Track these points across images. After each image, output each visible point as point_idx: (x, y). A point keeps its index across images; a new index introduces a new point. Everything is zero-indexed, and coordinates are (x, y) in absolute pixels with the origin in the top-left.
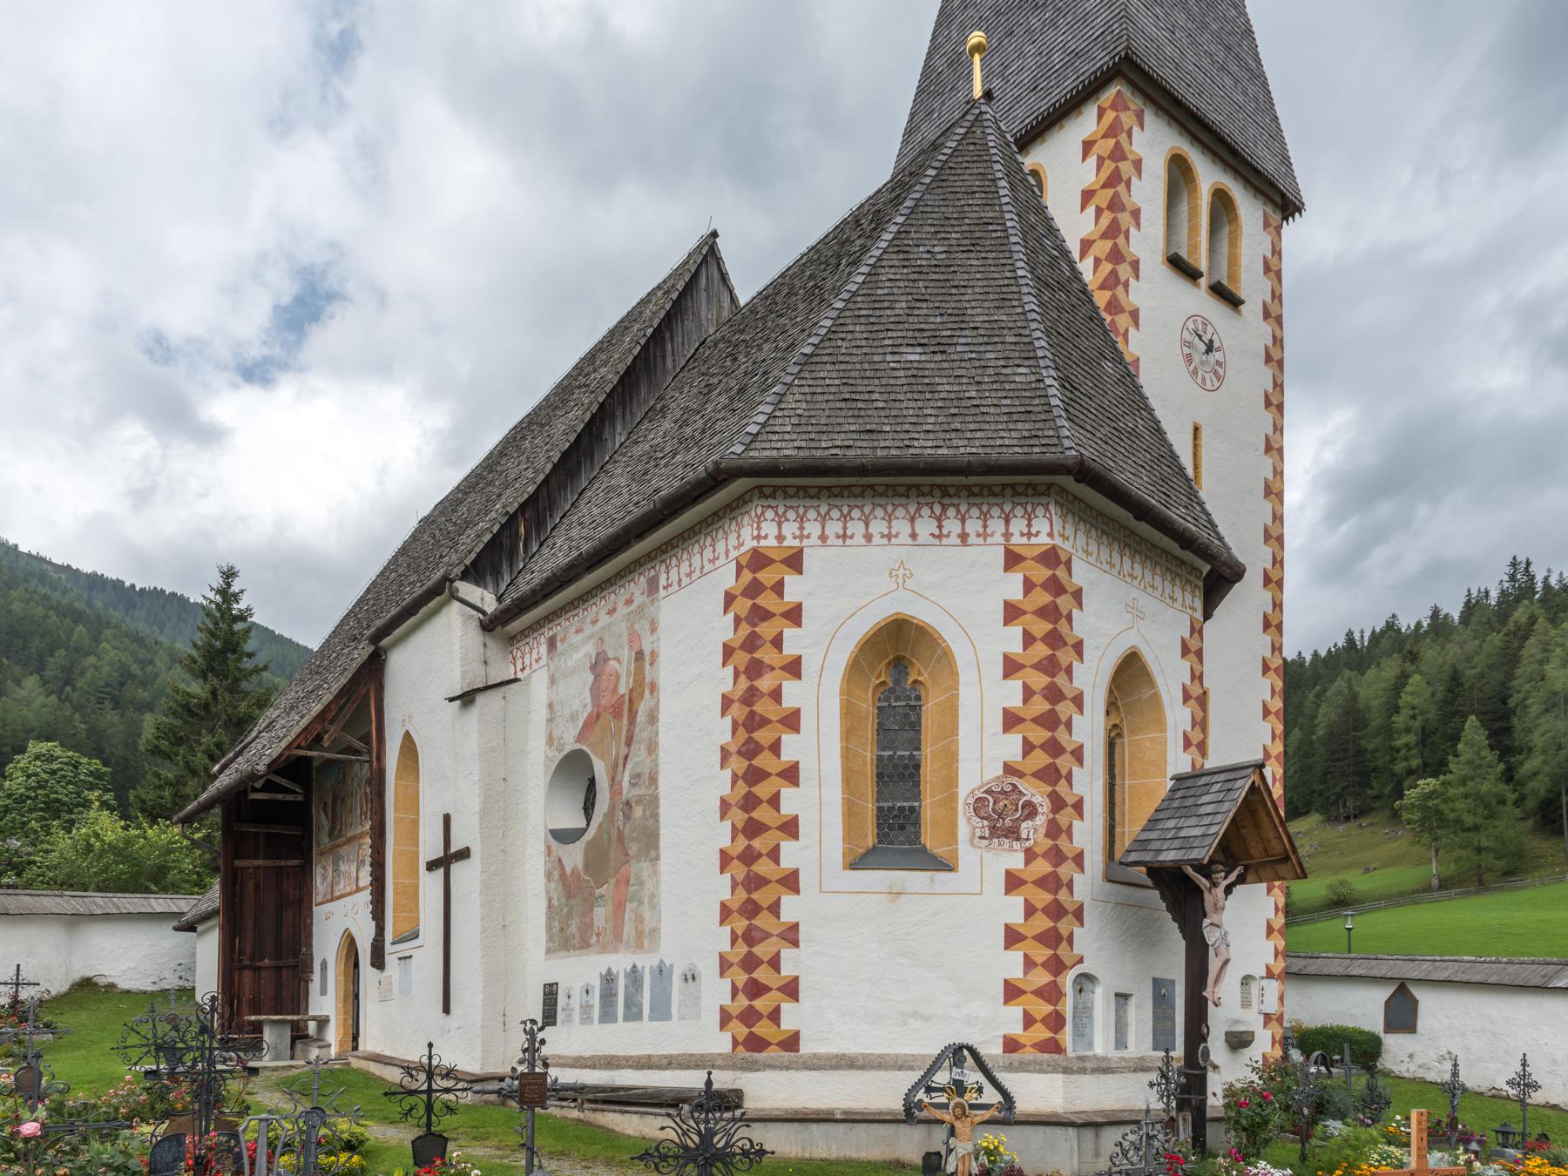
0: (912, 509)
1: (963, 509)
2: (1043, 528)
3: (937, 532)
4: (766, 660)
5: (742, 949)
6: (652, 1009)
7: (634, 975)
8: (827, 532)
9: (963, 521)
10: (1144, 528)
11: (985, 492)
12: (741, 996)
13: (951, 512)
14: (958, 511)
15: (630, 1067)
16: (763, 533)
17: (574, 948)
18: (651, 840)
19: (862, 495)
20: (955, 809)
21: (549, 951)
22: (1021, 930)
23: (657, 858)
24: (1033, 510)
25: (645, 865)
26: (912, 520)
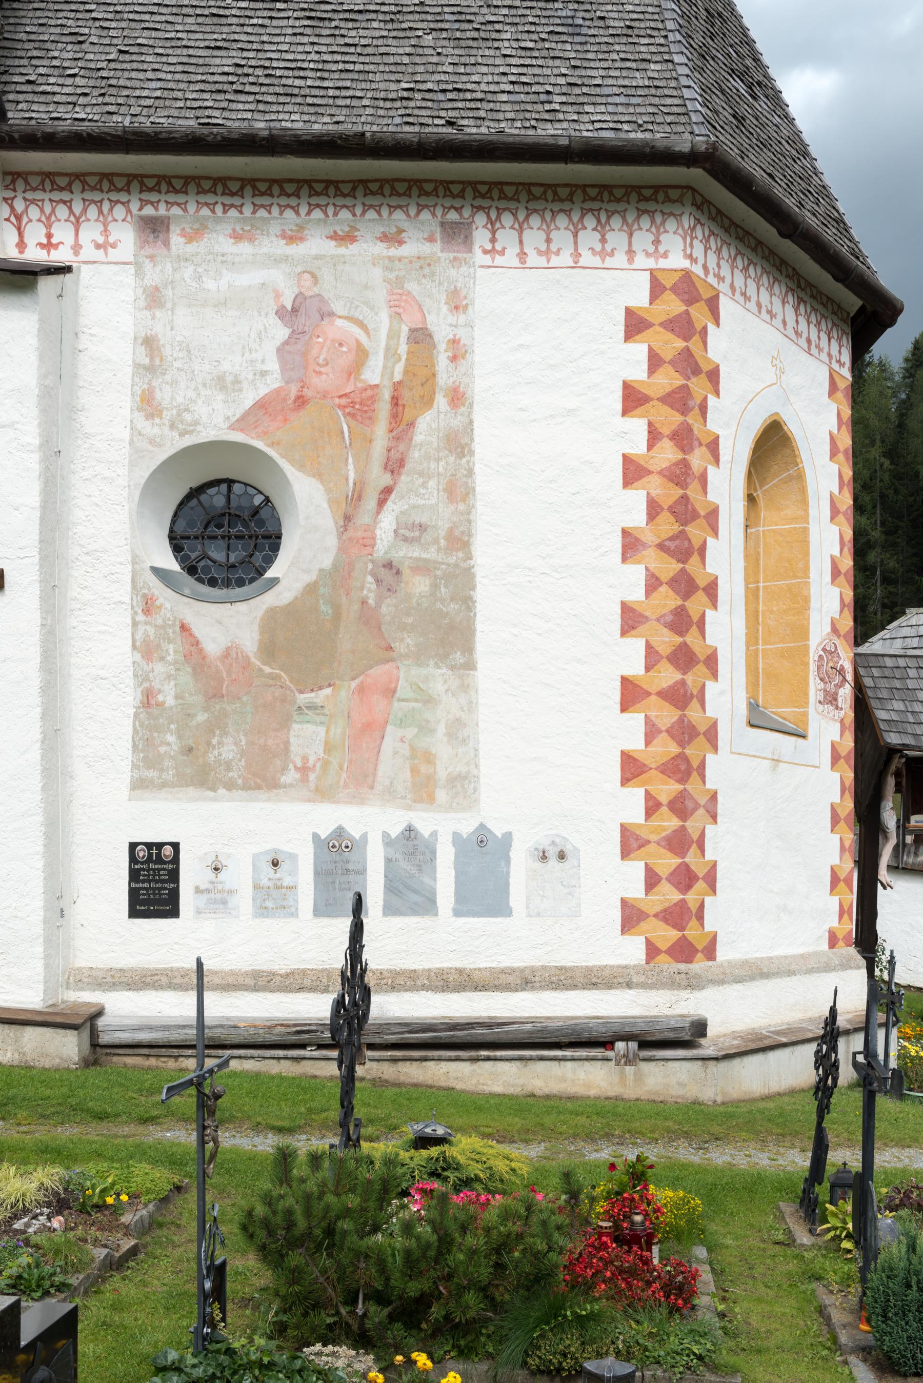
0: (576, 217)
1: (77, 207)
2: (678, 248)
3: (101, 240)
4: (666, 410)
5: (693, 826)
6: (461, 897)
7: (412, 847)
8: (81, 241)
9: (49, 226)
10: (788, 248)
11: (441, 191)
12: (693, 906)
13: (93, 211)
14: (101, 212)
15: (424, 988)
16: (111, 240)
17: (230, 786)
18: (452, 638)
19: (69, 188)
20: (806, 665)
21: (139, 785)
22: (642, 906)
23: (470, 665)
24: (498, 217)
25: (438, 679)
26: (521, 231)
